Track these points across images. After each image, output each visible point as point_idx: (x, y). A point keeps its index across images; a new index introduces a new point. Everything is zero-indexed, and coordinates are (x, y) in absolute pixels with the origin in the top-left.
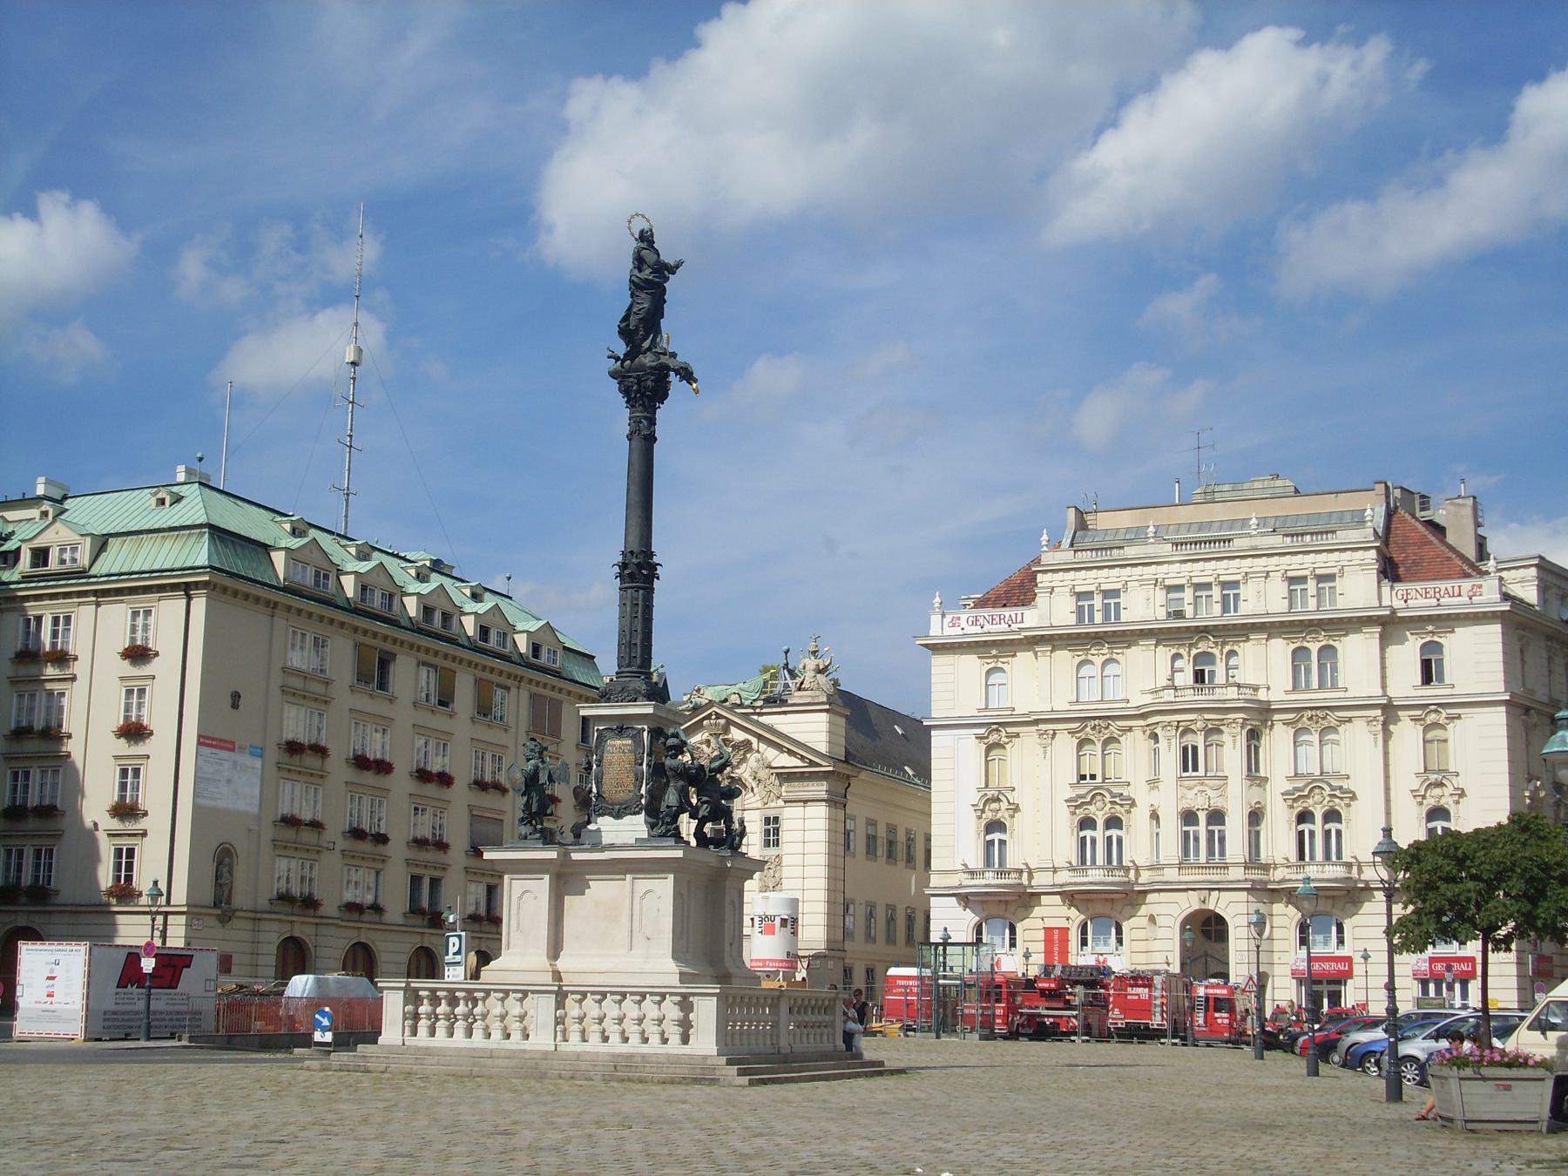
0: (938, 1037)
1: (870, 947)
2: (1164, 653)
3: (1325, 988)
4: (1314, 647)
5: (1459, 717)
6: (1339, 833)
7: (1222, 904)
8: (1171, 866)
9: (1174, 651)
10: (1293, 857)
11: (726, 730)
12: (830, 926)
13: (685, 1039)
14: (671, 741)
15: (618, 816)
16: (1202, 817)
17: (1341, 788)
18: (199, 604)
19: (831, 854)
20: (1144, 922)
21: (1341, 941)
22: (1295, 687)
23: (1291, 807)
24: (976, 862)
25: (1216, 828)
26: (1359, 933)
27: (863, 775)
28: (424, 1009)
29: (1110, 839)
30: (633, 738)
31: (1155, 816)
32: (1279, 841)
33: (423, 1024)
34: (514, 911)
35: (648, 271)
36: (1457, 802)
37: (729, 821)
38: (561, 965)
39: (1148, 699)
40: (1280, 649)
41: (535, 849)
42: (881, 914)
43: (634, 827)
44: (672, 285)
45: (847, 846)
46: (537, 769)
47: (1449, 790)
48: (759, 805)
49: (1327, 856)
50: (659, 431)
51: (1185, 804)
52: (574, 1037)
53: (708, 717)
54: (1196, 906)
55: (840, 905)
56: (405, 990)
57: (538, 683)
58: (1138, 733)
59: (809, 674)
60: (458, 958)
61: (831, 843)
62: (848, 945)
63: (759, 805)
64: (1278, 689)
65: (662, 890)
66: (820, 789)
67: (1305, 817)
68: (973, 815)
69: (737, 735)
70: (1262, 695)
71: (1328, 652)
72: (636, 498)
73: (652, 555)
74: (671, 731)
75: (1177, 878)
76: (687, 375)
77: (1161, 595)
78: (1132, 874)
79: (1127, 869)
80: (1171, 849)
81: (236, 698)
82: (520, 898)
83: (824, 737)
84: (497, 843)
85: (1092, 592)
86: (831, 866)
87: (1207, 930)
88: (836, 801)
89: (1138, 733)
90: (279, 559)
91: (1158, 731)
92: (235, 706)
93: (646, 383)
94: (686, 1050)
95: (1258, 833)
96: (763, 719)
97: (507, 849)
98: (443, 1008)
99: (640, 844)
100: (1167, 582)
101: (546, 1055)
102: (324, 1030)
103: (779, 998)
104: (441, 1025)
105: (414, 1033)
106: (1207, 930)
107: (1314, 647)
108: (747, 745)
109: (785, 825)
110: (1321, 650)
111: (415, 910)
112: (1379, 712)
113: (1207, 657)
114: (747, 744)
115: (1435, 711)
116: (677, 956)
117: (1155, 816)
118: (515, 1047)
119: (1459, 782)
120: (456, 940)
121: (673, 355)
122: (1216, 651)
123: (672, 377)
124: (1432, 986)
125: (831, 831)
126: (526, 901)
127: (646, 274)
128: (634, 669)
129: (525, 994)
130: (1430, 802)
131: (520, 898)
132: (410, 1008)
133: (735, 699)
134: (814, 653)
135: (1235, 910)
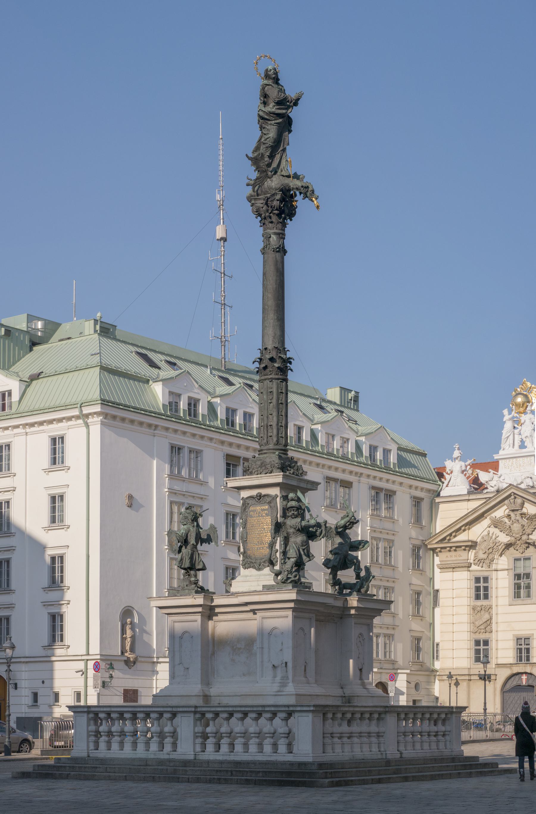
18: (96, 428)
30: (269, 503)
35: (271, 105)
37: (358, 570)
38: (213, 691)
42: (13, 606)
50: (288, 244)
52: (210, 748)
57: (416, 488)
72: (271, 303)
73: (285, 351)
93: (280, 207)
99: (267, 588)
121: (296, 176)
127: (271, 107)
128: (271, 446)
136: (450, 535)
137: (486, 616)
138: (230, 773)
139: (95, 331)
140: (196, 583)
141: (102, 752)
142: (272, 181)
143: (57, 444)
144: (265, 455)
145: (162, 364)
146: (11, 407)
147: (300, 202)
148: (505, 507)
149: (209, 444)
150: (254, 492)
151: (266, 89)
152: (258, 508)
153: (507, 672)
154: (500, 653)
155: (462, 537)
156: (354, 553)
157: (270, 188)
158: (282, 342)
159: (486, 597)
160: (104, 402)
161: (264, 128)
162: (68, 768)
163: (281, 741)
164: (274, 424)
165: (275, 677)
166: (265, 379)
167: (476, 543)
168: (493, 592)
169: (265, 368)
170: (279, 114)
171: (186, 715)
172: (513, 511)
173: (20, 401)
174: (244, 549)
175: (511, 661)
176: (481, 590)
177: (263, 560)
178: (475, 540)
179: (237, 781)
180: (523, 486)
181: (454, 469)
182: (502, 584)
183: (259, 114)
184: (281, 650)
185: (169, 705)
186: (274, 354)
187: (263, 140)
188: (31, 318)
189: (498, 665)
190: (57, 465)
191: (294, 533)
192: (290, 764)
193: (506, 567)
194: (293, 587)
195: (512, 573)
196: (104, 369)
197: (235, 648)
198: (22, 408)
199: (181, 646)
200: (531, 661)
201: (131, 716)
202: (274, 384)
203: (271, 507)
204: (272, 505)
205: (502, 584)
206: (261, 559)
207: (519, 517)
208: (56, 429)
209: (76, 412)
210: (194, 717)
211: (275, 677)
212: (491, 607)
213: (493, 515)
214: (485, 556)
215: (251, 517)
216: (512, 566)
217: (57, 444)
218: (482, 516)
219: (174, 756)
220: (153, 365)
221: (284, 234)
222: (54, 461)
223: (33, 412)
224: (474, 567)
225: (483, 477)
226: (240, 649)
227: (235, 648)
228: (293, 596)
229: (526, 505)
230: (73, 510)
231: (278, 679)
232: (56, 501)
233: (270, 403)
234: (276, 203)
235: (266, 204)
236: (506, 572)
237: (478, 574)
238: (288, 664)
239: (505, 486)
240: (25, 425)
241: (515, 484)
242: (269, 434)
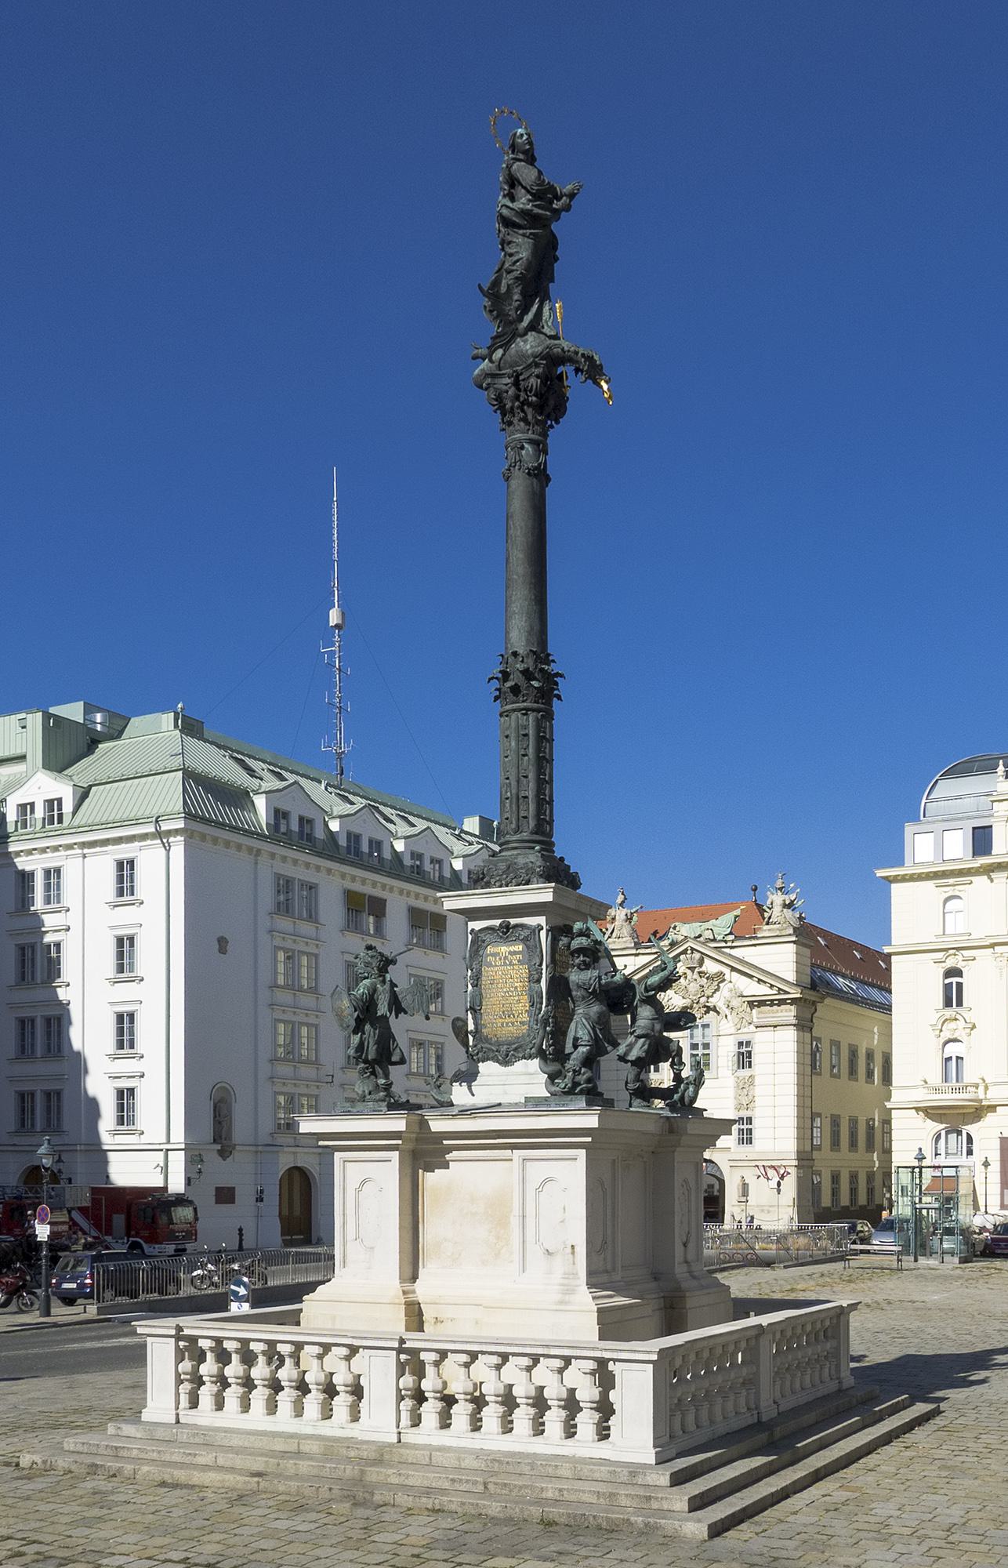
0: (916, 1260)
1: (835, 1155)
11: (701, 963)
12: (800, 1139)
13: (603, 1433)
14: (576, 943)
15: (506, 1061)
19: (800, 1074)
24: (936, 1078)
27: (828, 1001)
28: (209, 1368)
30: (525, 940)
33: (206, 1393)
34: (350, 1211)
37: (677, 1064)
38: (423, 1290)
41: (375, 1112)
43: (527, 1078)
45: (813, 1066)
46: (373, 991)
48: (733, 1031)
53: (685, 952)
55: (808, 1114)
56: (178, 1338)
59: (777, 910)
61: (800, 1063)
62: (816, 1154)
63: (733, 1031)
65: (569, 1175)
66: (789, 1013)
68: (933, 1034)
69: (710, 967)
74: (578, 926)
81: (223, 944)
82: (359, 1190)
83: (793, 966)
84: (317, 1109)
86: (800, 1085)
88: (804, 1025)
90: (260, 802)
92: (223, 950)
94: (603, 1450)
96: (733, 952)
97: (330, 1112)
98: (234, 1369)
99: (534, 1105)
101: (381, 1456)
103: (757, 1337)
104: (232, 1395)
108: (720, 978)
109: (756, 1050)
114: (721, 974)
116: (597, 1278)
118: (339, 1433)
125: (800, 1053)
126: (364, 1194)
128: (525, 835)
129: (354, 1350)
131: (359, 1190)
132: (186, 1365)
133: (708, 935)
134: (781, 889)
139: (176, 726)
140: (388, 1087)
142: (525, 342)
143: (125, 871)
144: (515, 852)
145: (266, 775)
146: (60, 821)
147: (574, 384)
150: (497, 922)
151: (515, 167)
152: (504, 949)
156: (673, 1035)
157: (523, 356)
158: (542, 641)
160: (189, 816)
161: (510, 243)
164: (531, 794)
166: (514, 710)
169: (515, 690)
173: (74, 813)
174: (476, 1024)
183: (501, 215)
186: (530, 663)
187: (507, 265)
188: (89, 710)
190: (125, 898)
191: (584, 998)
194: (589, 1103)
196: (189, 775)
198: (77, 821)
204: (532, 943)
206: (510, 1044)
207: (696, 976)
208: (124, 851)
209: (151, 829)
215: (490, 965)
217: (125, 871)
220: (251, 772)
221: (545, 445)
222: (120, 893)
223: (91, 827)
228: (591, 1120)
229: (707, 961)
230: (149, 957)
232: (124, 946)
234: (534, 382)
235: (516, 384)
238: (577, 1249)
240: (83, 845)
242: (523, 814)
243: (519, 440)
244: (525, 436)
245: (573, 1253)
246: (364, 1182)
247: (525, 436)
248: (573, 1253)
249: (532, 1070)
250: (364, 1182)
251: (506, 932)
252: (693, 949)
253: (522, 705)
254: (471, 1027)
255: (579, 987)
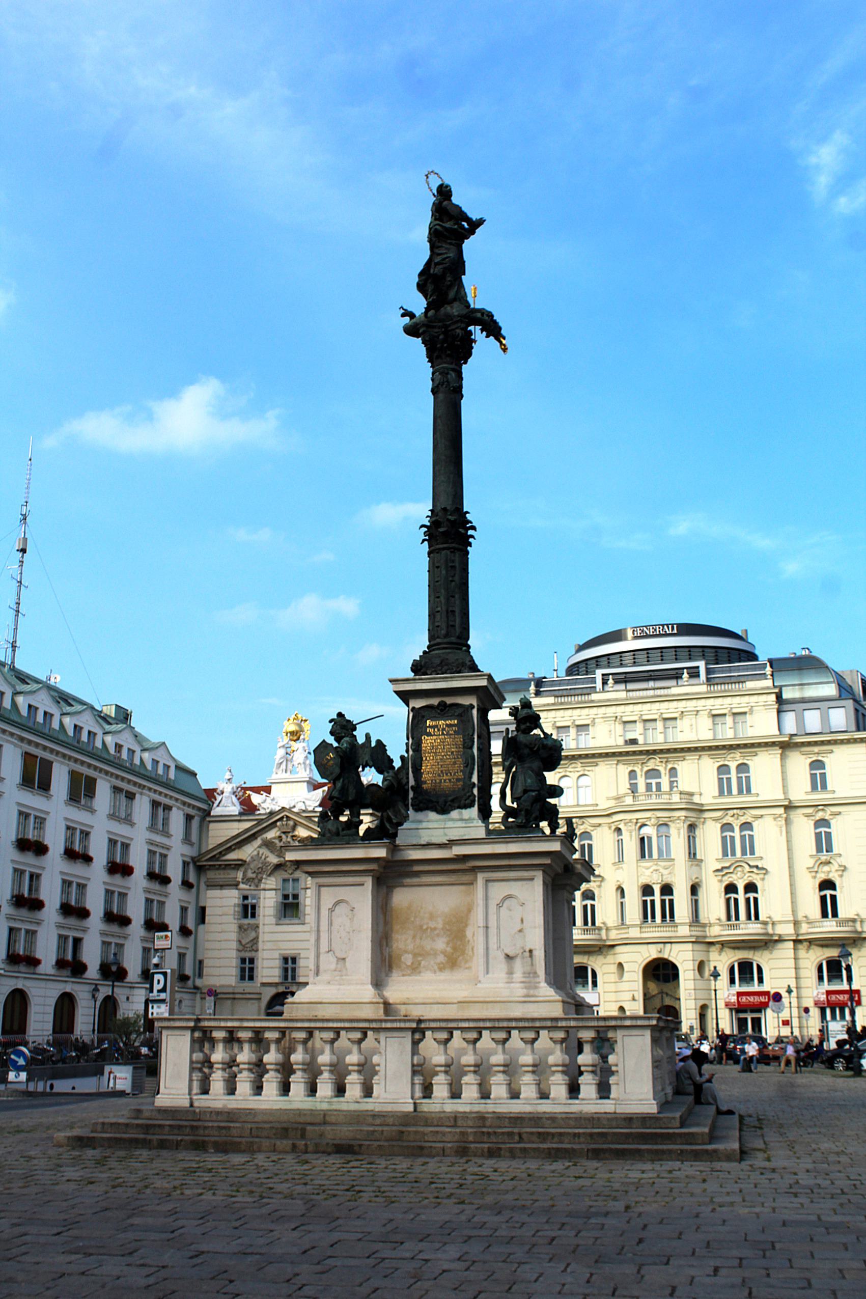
2: (624, 770)
3: (749, 1017)
4: (733, 765)
5: (840, 813)
6: (756, 900)
7: (673, 954)
8: (635, 926)
9: (630, 768)
10: (723, 916)
11: (294, 828)
13: (604, 1090)
16: (657, 890)
17: (757, 867)
20: (614, 968)
21: (761, 980)
22: (721, 793)
23: (721, 881)
25: (667, 898)
26: (775, 973)
28: (219, 1055)
29: (585, 907)
30: (459, 716)
31: (621, 891)
32: (713, 905)
36: (841, 876)
39: (612, 803)
40: (709, 766)
44: (472, 248)
47: (836, 867)
49: (749, 918)
51: (645, 880)
53: (281, 819)
54: (655, 955)
58: (605, 829)
60: (163, 996)
64: (708, 794)
67: (731, 888)
70: (696, 799)
71: (743, 768)
75: (639, 935)
76: (493, 329)
77: (619, 728)
78: (603, 932)
79: (600, 929)
80: (634, 912)
82: (331, 910)
85: (569, 727)
87: (661, 973)
89: (605, 829)
91: (621, 826)
95: (696, 901)
100: (625, 719)
101: (407, 1120)
102: (19, 1069)
105: (205, 1091)
106: (661, 973)
107: (733, 765)
110: (739, 766)
111: (61, 964)
112: (782, 810)
113: (653, 773)
115: (823, 810)
117: (621, 891)
119: (842, 861)
120: (161, 977)
122: (661, 769)
123: (476, 331)
124: (828, 1011)
130: (822, 876)
131: (331, 910)
135: (683, 958)
136: (220, 853)
137: (253, 935)
138: (517, 1138)
141: (217, 1098)
142: (452, 307)
148: (277, 829)
149: (9, 739)
150: (435, 701)
153: (272, 991)
154: (265, 972)
155: (232, 856)
159: (253, 915)
162: (167, 1128)
163: (524, 1078)
165: (510, 972)
166: (444, 549)
167: (245, 861)
168: (260, 911)
170: (451, 226)
171: (396, 1034)
172: (284, 833)
175: (277, 980)
176: (248, 910)
177: (450, 798)
178: (244, 859)
179: (550, 1153)
180: (295, 810)
181: (225, 790)
182: (268, 901)
184: (520, 931)
185: (319, 1017)
189: (263, 984)
192: (625, 1119)
193: (274, 887)
195: (280, 894)
197: (425, 927)
199: (331, 924)
200: (297, 980)
201: (227, 1035)
202: (457, 555)
203: (462, 721)
205: (268, 901)
207: (289, 839)
210: (192, 1037)
211: (510, 972)
212: (258, 927)
213: (264, 836)
214: (254, 876)
216: (280, 886)
218: (254, 837)
219: (369, 1105)
224: (242, 886)
225: (256, 799)
226: (435, 929)
227: (425, 927)
231: (518, 975)
233: (452, 581)
236: (274, 892)
237: (246, 893)
238: (535, 953)
239: (277, 809)
241: (288, 807)
242: (451, 623)
243: (447, 369)
244: (451, 366)
245: (531, 956)
246: (337, 903)
247: (451, 366)
248: (531, 956)
249: (470, 820)
250: (337, 903)
251: (442, 710)
252: (287, 817)
253: (451, 545)
254: (412, 782)
255: (526, 746)
